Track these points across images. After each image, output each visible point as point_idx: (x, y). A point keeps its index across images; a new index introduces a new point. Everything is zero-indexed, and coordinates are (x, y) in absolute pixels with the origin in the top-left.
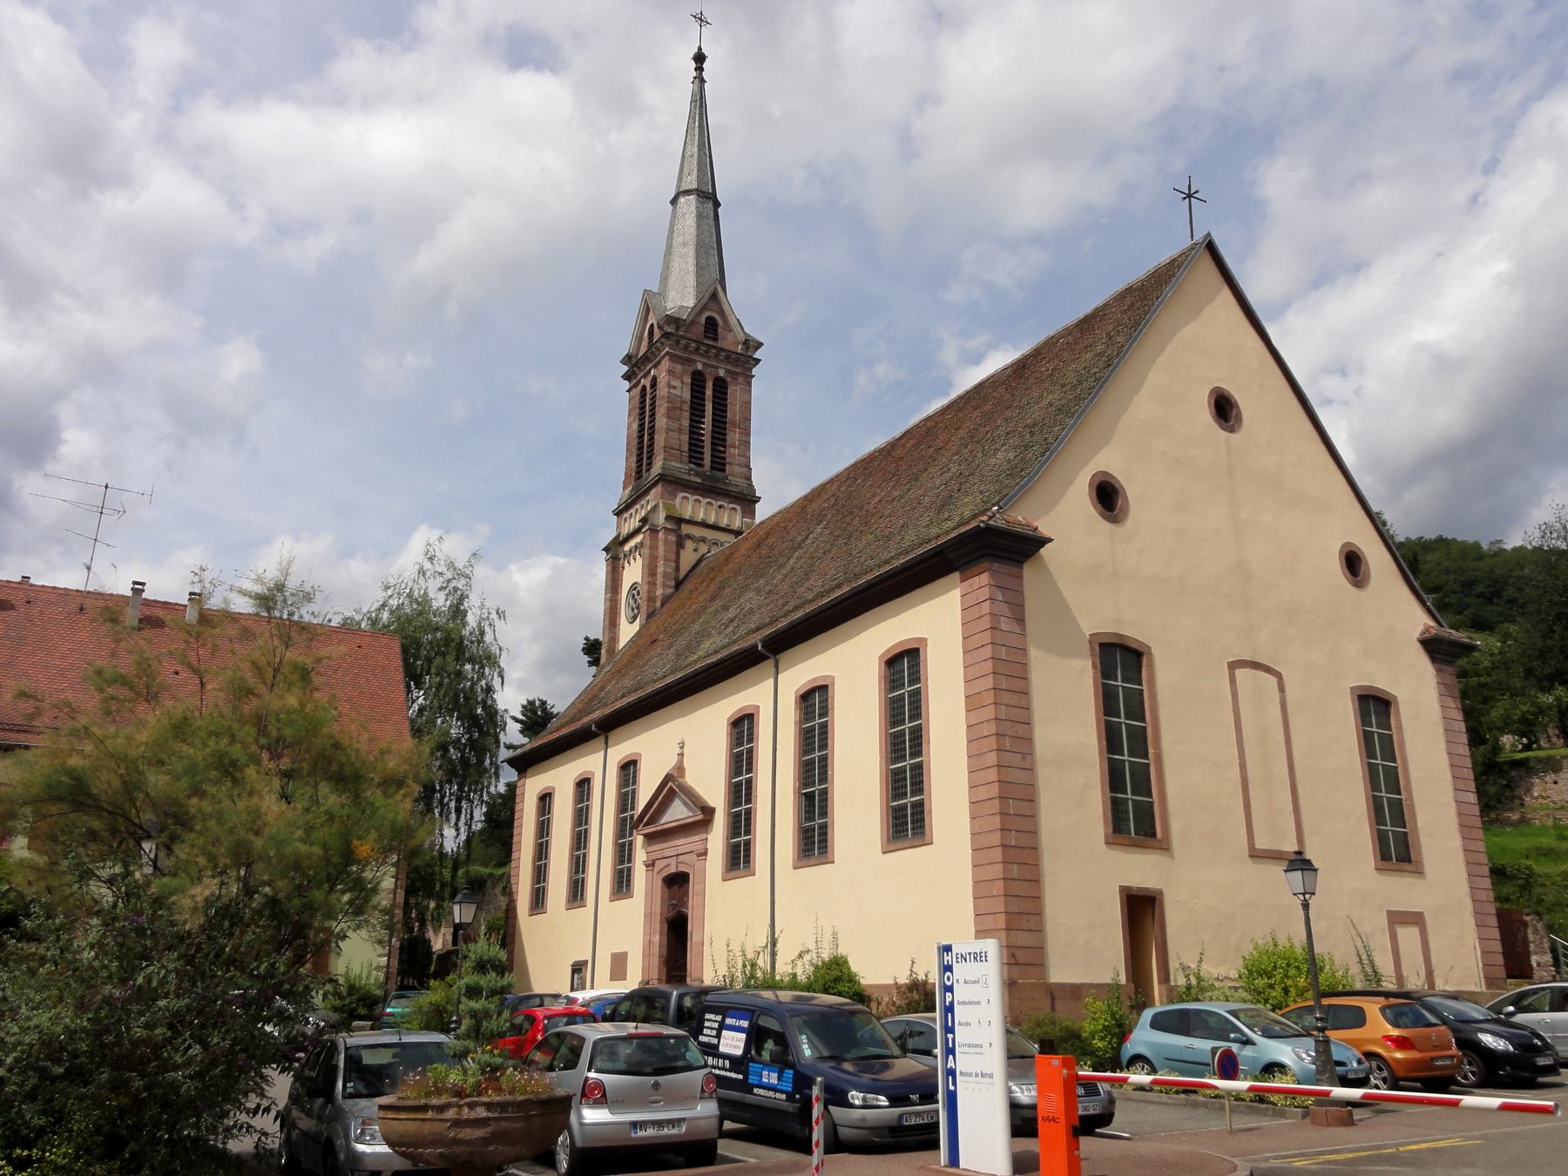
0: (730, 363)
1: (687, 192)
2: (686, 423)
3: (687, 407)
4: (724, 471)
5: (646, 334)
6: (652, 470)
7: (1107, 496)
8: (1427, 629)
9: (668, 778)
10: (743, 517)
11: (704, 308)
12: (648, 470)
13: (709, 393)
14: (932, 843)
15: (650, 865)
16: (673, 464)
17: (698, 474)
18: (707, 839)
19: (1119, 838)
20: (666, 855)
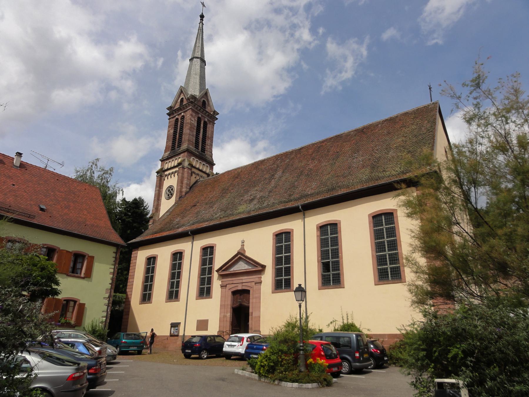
0: (209, 117)
1: (197, 58)
2: (195, 133)
3: (195, 128)
4: (205, 153)
5: (179, 101)
10: (210, 169)
11: (203, 97)
13: (202, 125)
14: (344, 288)
17: (198, 152)
18: (261, 277)
20: (234, 282)
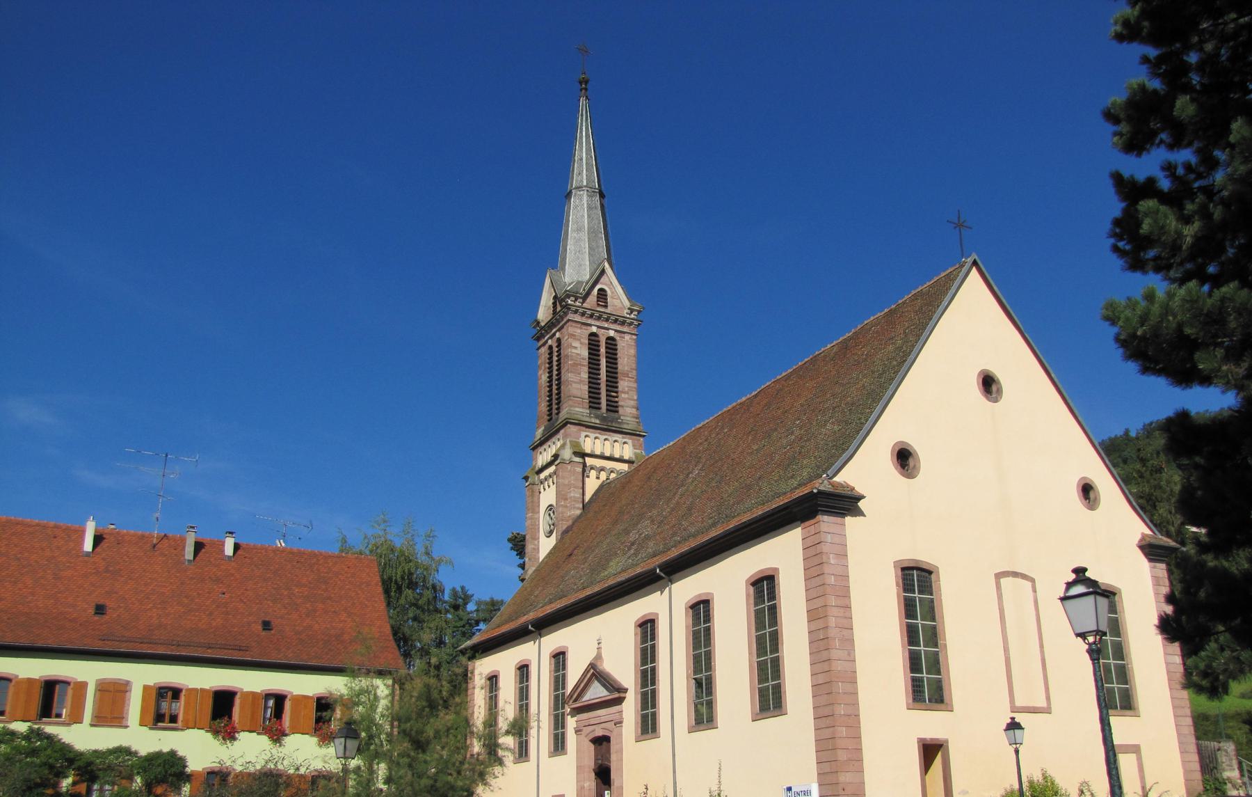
3: (586, 362)
4: (617, 412)
6: (561, 415)
7: (904, 457)
8: (1144, 536)
9: (592, 666)
12: (557, 414)
15: (578, 731)
16: (577, 409)
17: (597, 417)
19: (918, 705)
20: (592, 722)
